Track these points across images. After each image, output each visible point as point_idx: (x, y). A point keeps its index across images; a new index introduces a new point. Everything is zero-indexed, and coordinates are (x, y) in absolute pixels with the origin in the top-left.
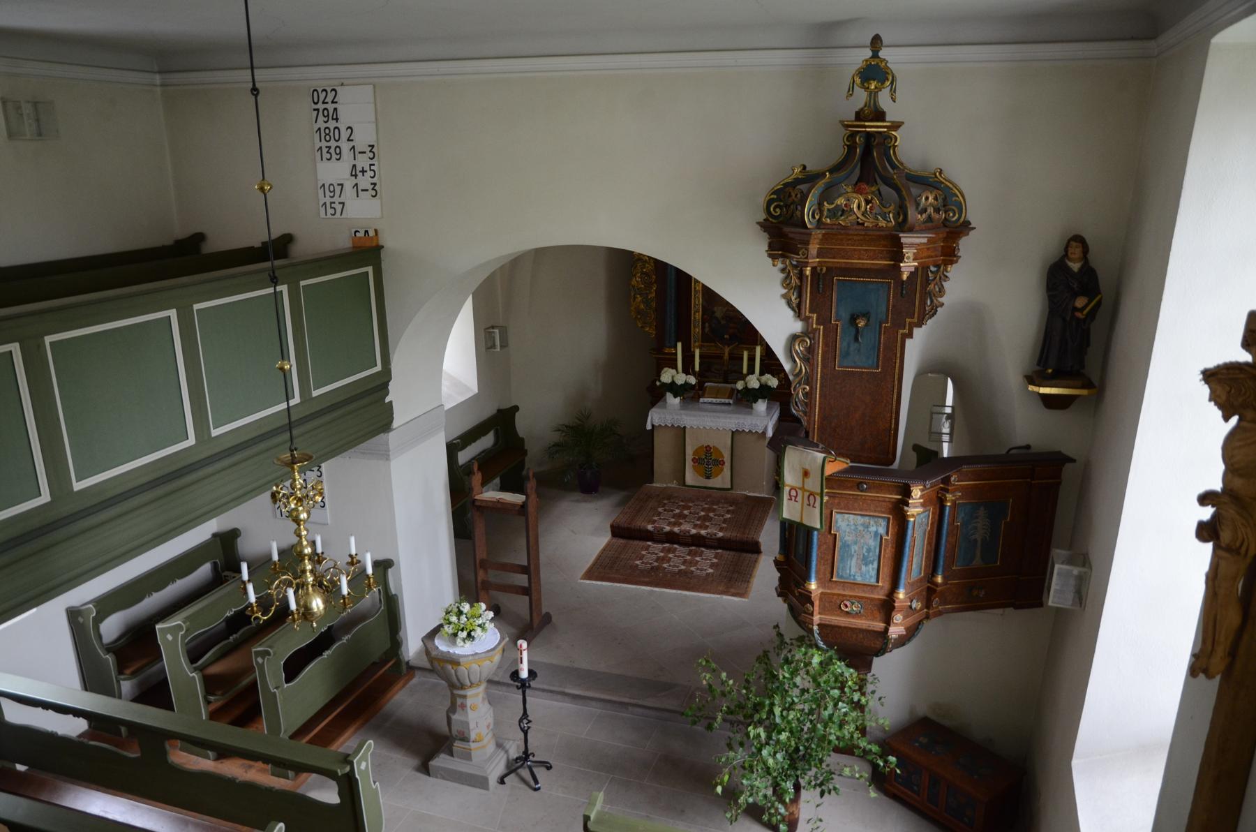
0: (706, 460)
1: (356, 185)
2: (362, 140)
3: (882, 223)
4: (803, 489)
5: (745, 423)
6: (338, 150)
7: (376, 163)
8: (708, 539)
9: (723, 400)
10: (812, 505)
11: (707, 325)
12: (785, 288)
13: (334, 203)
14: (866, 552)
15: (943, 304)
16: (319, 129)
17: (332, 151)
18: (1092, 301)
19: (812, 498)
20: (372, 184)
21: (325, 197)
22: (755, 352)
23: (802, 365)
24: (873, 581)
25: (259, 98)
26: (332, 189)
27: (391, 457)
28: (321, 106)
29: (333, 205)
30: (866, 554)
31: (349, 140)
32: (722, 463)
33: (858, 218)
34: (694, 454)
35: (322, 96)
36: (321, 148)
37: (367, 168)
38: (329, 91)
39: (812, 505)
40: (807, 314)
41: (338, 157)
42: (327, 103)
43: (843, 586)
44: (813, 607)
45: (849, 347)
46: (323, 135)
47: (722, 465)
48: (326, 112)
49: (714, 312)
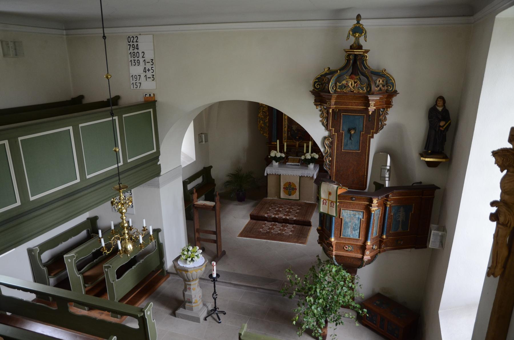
0: (289, 188)
1: (146, 75)
2: (148, 57)
4: (328, 200)
5: (305, 173)
6: (138, 61)
7: (154, 67)
8: (290, 220)
9: (296, 164)
10: (332, 206)
11: (289, 133)
12: (321, 118)
13: (137, 83)
14: (354, 226)
15: (386, 124)
16: (131, 53)
17: (136, 62)
18: (447, 123)
19: (332, 204)
20: (152, 75)
21: (133, 80)
22: (309, 144)
23: (328, 149)
24: (357, 237)
25: (106, 40)
26: (136, 77)
27: (160, 187)
28: (131, 43)
29: (136, 84)
30: (354, 226)
31: (143, 57)
32: (295, 189)
33: (351, 89)
34: (284, 186)
35: (132, 39)
36: (131, 60)
37: (150, 69)
38: (135, 37)
39: (332, 206)
40: (330, 128)
41: (138, 64)
42: (134, 42)
43: (345, 240)
44: (333, 248)
45: (347, 142)
46: (132, 55)
47: (296, 190)
48: (133, 46)
49: (292, 128)
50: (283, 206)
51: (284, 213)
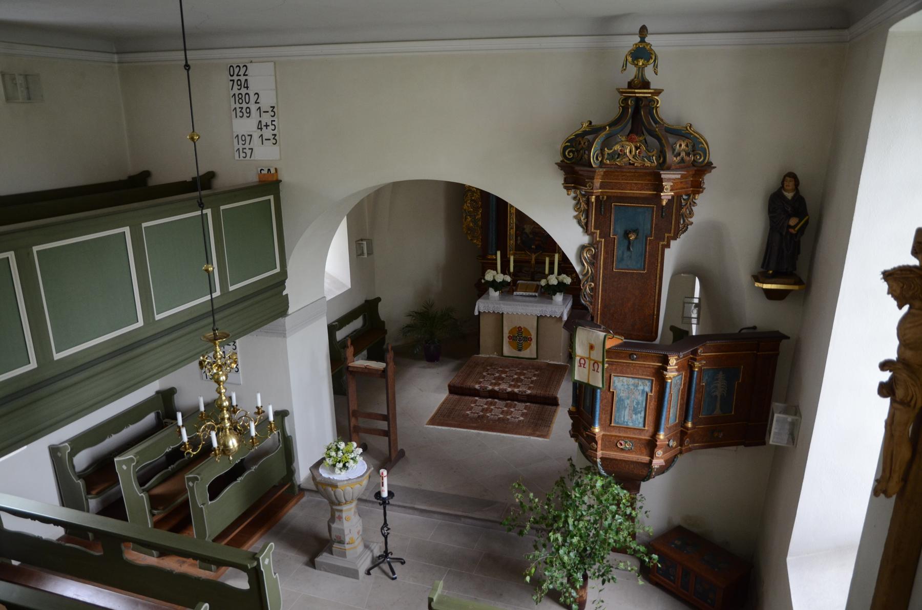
0: (518, 337)
1: (262, 135)
2: (265, 103)
3: (648, 164)
4: (589, 358)
5: (547, 310)
6: (248, 110)
7: (276, 120)
8: (520, 395)
9: (531, 294)
10: (596, 370)
11: (519, 238)
12: (576, 211)
13: (245, 149)
14: (636, 405)
15: (692, 223)
16: (234, 95)
17: (244, 110)
18: (801, 221)
19: (596, 365)
20: (273, 135)
21: (238, 144)
22: (554, 258)
23: (589, 268)
24: (641, 426)
25: (190, 71)
26: (243, 138)
27: (287, 335)
29: (244, 151)
30: (636, 406)
31: (256, 103)
32: (530, 339)
33: (630, 160)
34: (509, 333)
35: (237, 70)
36: (235, 108)
37: (269, 123)
38: (241, 67)
39: (596, 370)
40: (593, 230)
41: (248, 115)
42: (240, 75)
43: (619, 430)
44: (597, 445)
45: (623, 254)
46: (237, 99)
47: (530, 341)
48: (239, 82)
49: (524, 229)
50: (507, 370)
51: (509, 383)
